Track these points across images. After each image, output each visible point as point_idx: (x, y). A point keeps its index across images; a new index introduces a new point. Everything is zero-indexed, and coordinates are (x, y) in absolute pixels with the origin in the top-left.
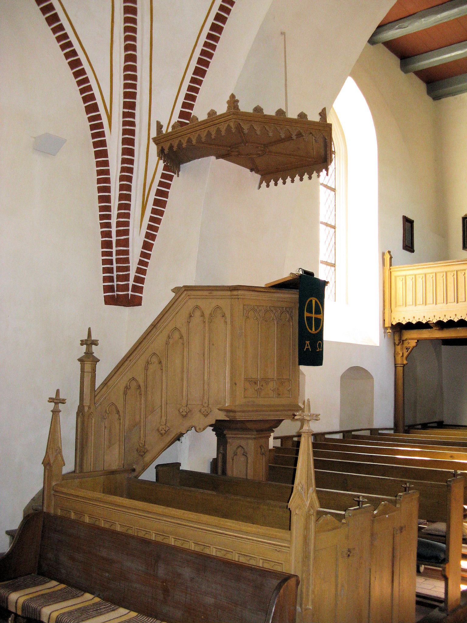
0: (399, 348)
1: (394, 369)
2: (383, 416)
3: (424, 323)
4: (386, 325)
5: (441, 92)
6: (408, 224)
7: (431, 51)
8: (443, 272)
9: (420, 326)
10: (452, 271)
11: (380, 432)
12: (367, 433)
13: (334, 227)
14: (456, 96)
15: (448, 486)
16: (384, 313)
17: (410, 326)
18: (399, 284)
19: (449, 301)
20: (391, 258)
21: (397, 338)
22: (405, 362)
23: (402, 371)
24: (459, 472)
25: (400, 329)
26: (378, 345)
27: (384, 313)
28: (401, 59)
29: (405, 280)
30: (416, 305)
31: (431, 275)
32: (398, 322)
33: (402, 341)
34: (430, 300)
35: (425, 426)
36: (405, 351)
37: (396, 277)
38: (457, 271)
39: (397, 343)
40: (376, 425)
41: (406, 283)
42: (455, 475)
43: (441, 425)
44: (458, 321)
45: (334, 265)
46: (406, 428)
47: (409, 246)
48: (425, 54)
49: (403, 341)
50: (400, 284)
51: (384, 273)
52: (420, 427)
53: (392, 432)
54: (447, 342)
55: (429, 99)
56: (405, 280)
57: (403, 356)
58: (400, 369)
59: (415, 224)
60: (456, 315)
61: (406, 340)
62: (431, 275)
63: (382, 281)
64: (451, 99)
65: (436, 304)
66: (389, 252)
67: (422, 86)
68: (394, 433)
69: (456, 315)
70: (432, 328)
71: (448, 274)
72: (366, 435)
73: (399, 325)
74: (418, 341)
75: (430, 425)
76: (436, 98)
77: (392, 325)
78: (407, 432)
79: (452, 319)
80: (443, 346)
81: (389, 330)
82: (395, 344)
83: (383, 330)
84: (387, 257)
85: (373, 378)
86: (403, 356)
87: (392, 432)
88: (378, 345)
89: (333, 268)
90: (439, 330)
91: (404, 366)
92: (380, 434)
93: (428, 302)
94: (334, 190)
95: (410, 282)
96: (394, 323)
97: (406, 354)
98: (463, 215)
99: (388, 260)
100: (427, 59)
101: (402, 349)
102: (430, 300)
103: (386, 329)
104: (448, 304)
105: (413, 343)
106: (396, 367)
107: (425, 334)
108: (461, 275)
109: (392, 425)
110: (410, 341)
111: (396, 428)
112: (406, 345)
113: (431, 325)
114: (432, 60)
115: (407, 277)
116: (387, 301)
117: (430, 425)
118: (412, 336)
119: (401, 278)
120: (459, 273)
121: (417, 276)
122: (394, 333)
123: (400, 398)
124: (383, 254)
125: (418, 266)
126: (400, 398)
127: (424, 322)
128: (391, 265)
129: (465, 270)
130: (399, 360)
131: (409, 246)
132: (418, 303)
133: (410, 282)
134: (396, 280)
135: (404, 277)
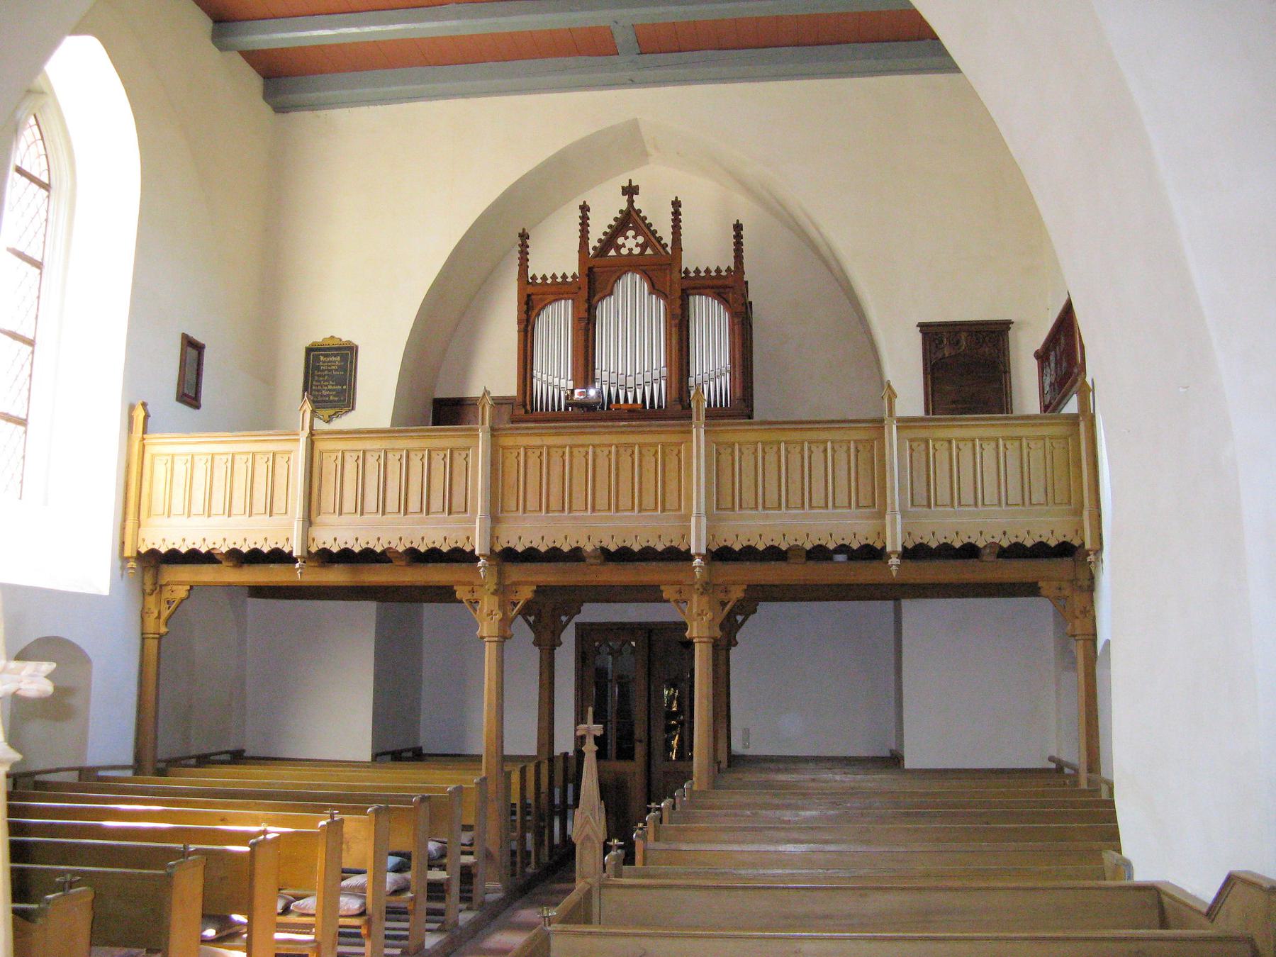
0: (151, 600)
1: (138, 642)
2: (108, 737)
3: (737, 549)
4: (128, 553)
5: (294, 98)
6: (192, 353)
7: (275, 17)
8: (267, 453)
9: (194, 557)
10: (265, 453)
11: (101, 773)
12: (72, 777)
13: (31, 343)
14: (319, 113)
15: (169, 875)
16: (123, 528)
17: (174, 557)
18: (159, 472)
19: (254, 511)
20: (147, 417)
21: (149, 579)
22: (163, 630)
23: (155, 650)
24: (192, 847)
25: (156, 562)
26: (106, 592)
27: (123, 528)
28: (215, 22)
29: (173, 462)
30: (230, 515)
31: (224, 458)
32: (151, 547)
33: (158, 588)
34: (218, 506)
35: (204, 760)
36: (164, 606)
37: (153, 456)
38: (274, 454)
39: (148, 591)
40: (91, 761)
41: (172, 469)
42: (185, 854)
43: (238, 757)
44: (547, 552)
45: (22, 422)
46: (162, 765)
47: (190, 395)
48: (248, 23)
49: (161, 586)
50: (160, 471)
51: (129, 446)
52: (193, 761)
53: (129, 773)
54: (258, 591)
55: (268, 109)
56: (173, 462)
57: (159, 617)
58: (152, 645)
59: (207, 354)
60: (1005, 533)
61: (167, 585)
62: (224, 458)
63: (123, 465)
64: (307, 115)
65: (230, 515)
66: (144, 405)
67: (255, 82)
68: (135, 774)
69: (1005, 533)
70: (219, 562)
71: (258, 457)
72: (69, 780)
73: (153, 553)
74: (192, 587)
75: (218, 757)
76: (280, 109)
77: (139, 553)
78: (161, 773)
79: (258, 546)
80: (250, 600)
81: (132, 564)
82: (143, 591)
83: (119, 564)
84: (139, 414)
85: (89, 661)
86: (159, 617)
87: (129, 773)
88: (106, 592)
89: (21, 429)
90: (235, 566)
91: (160, 637)
92: (100, 779)
93: (213, 511)
94: (38, 265)
95: (180, 468)
96: (143, 550)
97: (166, 613)
98: (308, 343)
99: (140, 421)
100: (265, 32)
101: (158, 603)
102: (218, 506)
103: (125, 560)
104: (274, 517)
105: (181, 592)
106: (143, 639)
107: (206, 574)
108: (281, 461)
109: (129, 760)
110: (175, 587)
111: (138, 766)
112: (166, 594)
113: (218, 557)
114: (275, 36)
115: (176, 458)
116: (131, 503)
117: (218, 757)
118: (184, 574)
119: (204, 458)
120: (278, 457)
121: (196, 458)
122: (144, 569)
123: (150, 706)
124: (132, 408)
125: (204, 436)
126: (150, 706)
127: (379, 549)
128: (145, 432)
129: (290, 452)
130: (151, 626)
131: (190, 395)
132: (194, 510)
133: (180, 468)
134: (153, 463)
135: (170, 458)
